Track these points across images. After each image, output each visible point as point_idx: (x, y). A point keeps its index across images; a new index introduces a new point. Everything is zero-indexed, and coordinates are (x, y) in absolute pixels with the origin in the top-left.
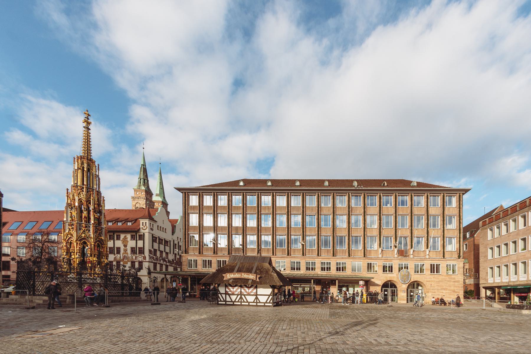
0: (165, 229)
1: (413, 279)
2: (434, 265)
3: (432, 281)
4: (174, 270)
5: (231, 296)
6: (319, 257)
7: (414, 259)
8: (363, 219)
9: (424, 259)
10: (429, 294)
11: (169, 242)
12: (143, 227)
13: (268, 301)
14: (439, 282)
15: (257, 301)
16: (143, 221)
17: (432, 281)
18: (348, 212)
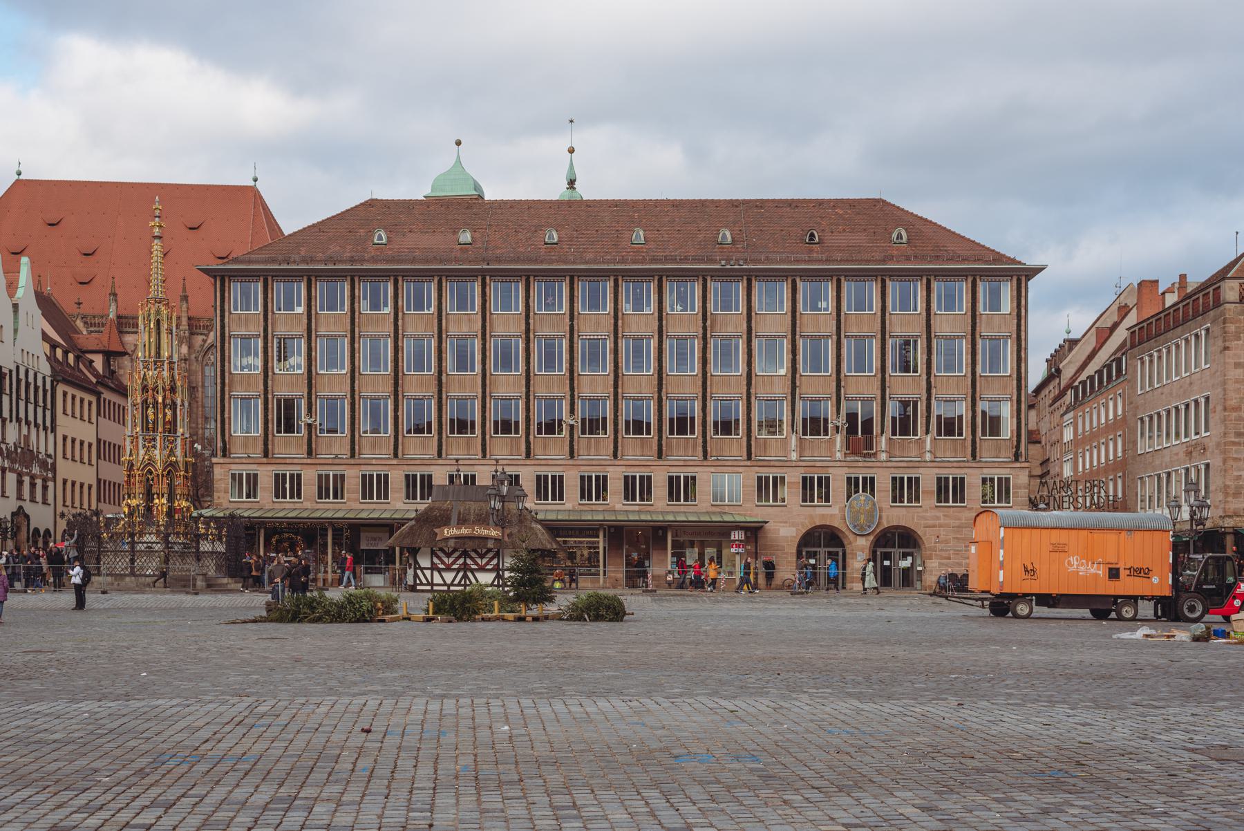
1: (888, 522)
2: (634, 478)
3: (940, 526)
5: (444, 574)
6: (617, 462)
7: (889, 464)
8: (746, 350)
9: (917, 464)
10: (933, 564)
11: (8, 377)
13: (456, 582)
14: (958, 527)
15: (465, 582)
17: (940, 526)
18: (701, 331)
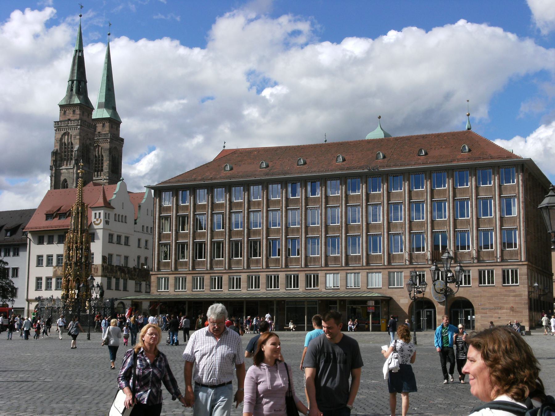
0: (126, 217)
3: (481, 296)
4: (142, 302)
9: (468, 265)
12: (95, 220)
16: (96, 212)
